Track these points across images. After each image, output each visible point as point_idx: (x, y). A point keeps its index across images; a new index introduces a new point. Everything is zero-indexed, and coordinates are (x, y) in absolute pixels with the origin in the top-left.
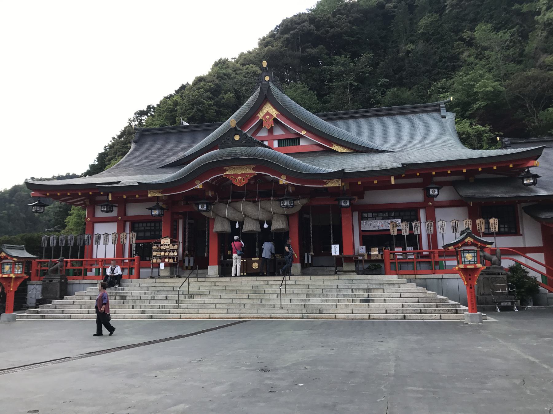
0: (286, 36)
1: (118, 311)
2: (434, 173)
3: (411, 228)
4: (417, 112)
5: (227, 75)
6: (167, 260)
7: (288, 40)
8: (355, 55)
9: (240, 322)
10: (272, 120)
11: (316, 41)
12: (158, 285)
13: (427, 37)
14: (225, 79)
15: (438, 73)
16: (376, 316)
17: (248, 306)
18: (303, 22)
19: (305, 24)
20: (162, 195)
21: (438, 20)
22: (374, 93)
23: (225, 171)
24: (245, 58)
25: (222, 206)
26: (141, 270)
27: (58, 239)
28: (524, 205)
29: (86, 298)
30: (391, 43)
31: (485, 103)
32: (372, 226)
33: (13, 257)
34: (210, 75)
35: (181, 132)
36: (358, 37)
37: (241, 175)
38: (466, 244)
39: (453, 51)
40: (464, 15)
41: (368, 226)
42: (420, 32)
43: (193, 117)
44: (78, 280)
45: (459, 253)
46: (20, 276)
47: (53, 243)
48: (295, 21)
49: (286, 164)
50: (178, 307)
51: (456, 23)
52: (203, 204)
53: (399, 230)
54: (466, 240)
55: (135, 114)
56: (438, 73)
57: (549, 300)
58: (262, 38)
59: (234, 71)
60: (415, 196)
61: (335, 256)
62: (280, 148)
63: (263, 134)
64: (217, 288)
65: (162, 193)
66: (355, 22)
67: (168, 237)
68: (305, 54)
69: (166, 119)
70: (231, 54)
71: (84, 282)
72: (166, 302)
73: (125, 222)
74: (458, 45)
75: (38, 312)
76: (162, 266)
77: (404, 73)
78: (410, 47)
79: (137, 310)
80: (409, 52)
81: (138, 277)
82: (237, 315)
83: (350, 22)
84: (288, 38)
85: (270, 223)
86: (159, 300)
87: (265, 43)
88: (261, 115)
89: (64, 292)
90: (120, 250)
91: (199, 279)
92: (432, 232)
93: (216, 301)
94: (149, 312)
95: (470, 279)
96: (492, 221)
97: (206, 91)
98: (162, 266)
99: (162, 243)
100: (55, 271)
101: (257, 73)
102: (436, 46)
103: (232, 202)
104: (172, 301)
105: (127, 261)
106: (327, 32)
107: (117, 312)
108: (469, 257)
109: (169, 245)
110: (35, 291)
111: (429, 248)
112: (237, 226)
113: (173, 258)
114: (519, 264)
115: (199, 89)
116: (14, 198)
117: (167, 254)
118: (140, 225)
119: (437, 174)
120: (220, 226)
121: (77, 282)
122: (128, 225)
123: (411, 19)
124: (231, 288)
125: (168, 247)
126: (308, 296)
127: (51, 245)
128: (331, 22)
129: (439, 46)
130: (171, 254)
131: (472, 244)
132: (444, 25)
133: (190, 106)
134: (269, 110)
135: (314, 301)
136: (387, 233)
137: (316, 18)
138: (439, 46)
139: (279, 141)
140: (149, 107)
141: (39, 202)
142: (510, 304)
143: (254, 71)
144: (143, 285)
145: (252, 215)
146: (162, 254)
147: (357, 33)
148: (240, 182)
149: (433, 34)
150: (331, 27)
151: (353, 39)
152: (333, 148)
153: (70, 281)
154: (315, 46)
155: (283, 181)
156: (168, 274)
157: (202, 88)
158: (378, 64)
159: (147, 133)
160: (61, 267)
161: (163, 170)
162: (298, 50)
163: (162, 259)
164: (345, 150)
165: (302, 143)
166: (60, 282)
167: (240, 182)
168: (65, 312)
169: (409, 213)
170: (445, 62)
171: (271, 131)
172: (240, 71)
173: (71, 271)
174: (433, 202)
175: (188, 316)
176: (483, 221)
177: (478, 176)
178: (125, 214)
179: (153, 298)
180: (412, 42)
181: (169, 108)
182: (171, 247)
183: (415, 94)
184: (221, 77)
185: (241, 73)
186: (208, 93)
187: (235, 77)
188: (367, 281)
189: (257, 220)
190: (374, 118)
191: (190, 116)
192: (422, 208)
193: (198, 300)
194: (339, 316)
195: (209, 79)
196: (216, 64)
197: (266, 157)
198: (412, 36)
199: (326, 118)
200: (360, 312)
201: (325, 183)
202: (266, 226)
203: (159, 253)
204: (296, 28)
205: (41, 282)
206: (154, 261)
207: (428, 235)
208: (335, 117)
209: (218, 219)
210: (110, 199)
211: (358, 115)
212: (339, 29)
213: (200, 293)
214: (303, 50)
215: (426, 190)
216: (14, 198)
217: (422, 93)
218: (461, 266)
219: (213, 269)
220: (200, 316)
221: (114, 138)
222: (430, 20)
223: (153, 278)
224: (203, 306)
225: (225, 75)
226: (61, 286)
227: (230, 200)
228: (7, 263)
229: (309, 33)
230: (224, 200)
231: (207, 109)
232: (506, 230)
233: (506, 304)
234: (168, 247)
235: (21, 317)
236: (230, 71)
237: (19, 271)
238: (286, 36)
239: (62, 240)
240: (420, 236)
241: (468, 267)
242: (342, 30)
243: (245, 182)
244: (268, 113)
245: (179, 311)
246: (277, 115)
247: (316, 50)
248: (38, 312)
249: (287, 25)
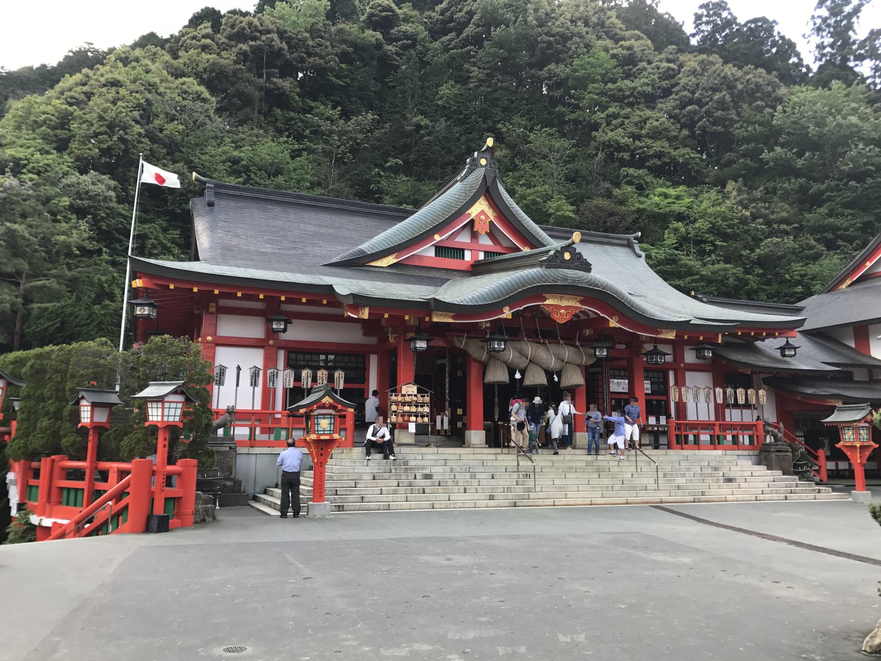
2: (283, 298)
20: (453, 321)
28: (763, 376)
29: (366, 478)
35: (240, 197)
36: (346, 82)
38: (323, 407)
43: (109, 149)
45: (312, 418)
46: (867, 444)
54: (324, 401)
65: (453, 318)
85: (523, 373)
90: (268, 395)
95: (321, 455)
96: (761, 392)
99: (404, 392)
101: (203, 96)
105: (279, 416)
107: (452, 498)
108: (324, 424)
109: (415, 396)
117: (414, 409)
119: (289, 301)
120: (498, 375)
122: (281, 354)
128: (308, 45)
130: (420, 409)
131: (331, 407)
143: (197, 93)
148: (561, 317)
150: (309, 55)
167: (561, 317)
168: (365, 500)
174: (277, 339)
176: (310, 372)
191: (105, 146)
199: (552, 233)
201: (659, 333)
202: (518, 376)
210: (720, 342)
215: (269, 321)
218: (314, 437)
219: (477, 436)
228: (324, 415)
234: (415, 399)
241: (322, 438)
242: (326, 63)
243: (568, 317)
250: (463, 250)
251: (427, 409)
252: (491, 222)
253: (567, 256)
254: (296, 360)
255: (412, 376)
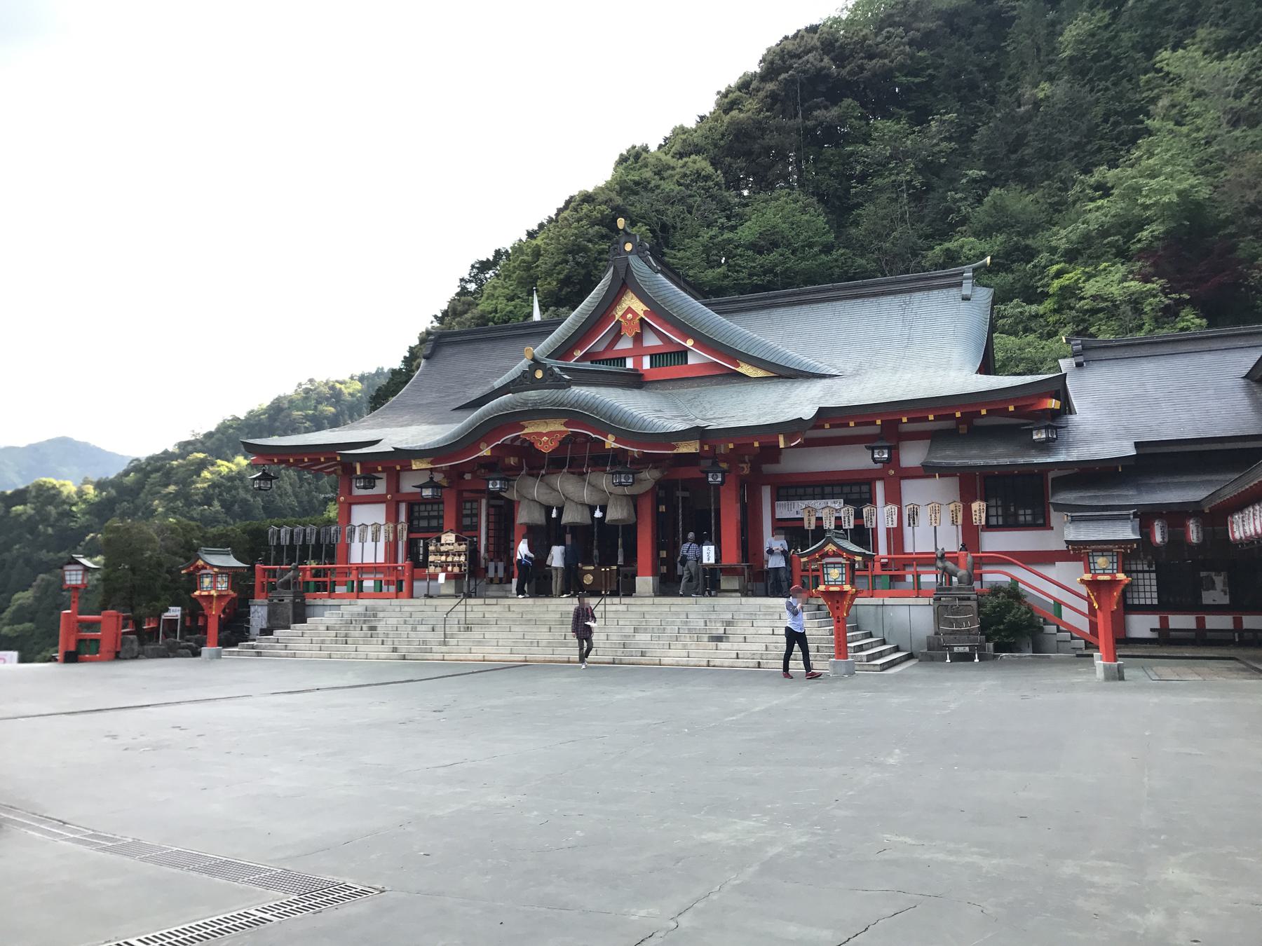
0: (771, 86)
1: (361, 648)
3: (858, 515)
4: (920, 289)
5: (642, 185)
6: (450, 568)
7: (773, 96)
8: (920, 118)
9: (525, 665)
10: (637, 321)
11: (834, 90)
12: (426, 609)
13: (1079, 68)
14: (637, 193)
15: (1100, 150)
16: (717, 662)
17: (543, 643)
18: (810, 51)
19: (810, 57)
21: (1107, 26)
22: (955, 201)
23: (523, 428)
24: (684, 141)
25: (530, 480)
26: (416, 584)
27: (292, 532)
30: (1006, 81)
31: (1162, 229)
32: (794, 510)
33: (213, 566)
34: (608, 187)
37: (547, 434)
39: (1138, 96)
40: (1168, 11)
41: (787, 511)
42: (1065, 54)
44: (321, 600)
47: (285, 540)
48: (789, 52)
49: (610, 418)
50: (445, 643)
51: (1148, 31)
52: (494, 479)
53: (819, 519)
55: (473, 267)
56: (1100, 150)
57: (1061, 644)
58: (723, 91)
59: (658, 173)
60: (856, 460)
61: (707, 565)
62: (655, 370)
63: (625, 344)
64: (510, 615)
66: (926, 40)
67: (452, 531)
68: (810, 123)
69: (519, 283)
70: (652, 136)
71: (330, 602)
72: (431, 635)
73: (398, 503)
74: (1148, 82)
75: (253, 647)
76: (442, 578)
77: (1029, 151)
78: (1044, 90)
79: (388, 646)
80: (1037, 104)
81: (412, 597)
82: (521, 657)
83: (910, 43)
84: (773, 92)
85: (603, 509)
86: (423, 632)
87: (729, 102)
88: (618, 313)
89: (300, 616)
91: (488, 601)
92: (895, 525)
93: (500, 635)
94: (403, 649)
97: (592, 225)
98: (442, 578)
100: (286, 585)
102: (1102, 85)
103: (547, 474)
104: (439, 635)
106: (861, 68)
110: (259, 614)
111: (889, 553)
112: (554, 515)
113: (460, 566)
114: (1015, 581)
115: (579, 220)
116: (278, 424)
117: (450, 559)
118: (423, 508)
121: (319, 602)
123: (1053, 24)
124: (529, 616)
125: (451, 547)
126: (636, 630)
127: (283, 543)
128: (870, 46)
129: (1109, 84)
130: (456, 559)
131: (835, 555)
132: (1123, 35)
133: (562, 256)
134: (632, 304)
135: (642, 638)
136: (797, 524)
137: (837, 41)
138: (1109, 84)
139: (654, 358)
140: (498, 253)
141: (264, 473)
142: (967, 649)
144: (406, 609)
145: (578, 497)
146: (443, 558)
147: (928, 67)
148: (546, 446)
149: (1096, 59)
150: (871, 57)
151: (917, 80)
152: (739, 370)
153: (309, 601)
154: (834, 100)
155: (610, 442)
156: (452, 591)
157: (587, 216)
158: (973, 130)
159: (448, 339)
160: (295, 578)
161: (459, 413)
162: (796, 115)
163: (443, 566)
164: (761, 373)
165: (692, 360)
166: (293, 602)
167: (546, 446)
169: (857, 490)
170: (1116, 124)
171: (638, 338)
172: (670, 172)
173: (312, 586)
175: (454, 656)
177: (978, 422)
178: (398, 490)
179: (414, 629)
180: (1051, 78)
181: (524, 261)
182: (456, 547)
183: (1041, 201)
184: (628, 188)
185: (672, 176)
186: (597, 227)
187: (657, 187)
188: (734, 608)
189: (583, 504)
190: (839, 303)
191: (561, 276)
192: (879, 479)
193: (476, 634)
194: (665, 660)
195: (601, 198)
196: (623, 160)
197: (579, 406)
198: (1051, 62)
199: (720, 307)
200: (701, 653)
201: (674, 447)
202: (598, 514)
203: (438, 557)
204: (791, 67)
205: (266, 602)
206: (432, 569)
207: (888, 530)
208: (768, 302)
209: (524, 504)
211: (811, 297)
212: (886, 61)
213: (483, 623)
214: (807, 115)
216: (278, 424)
217: (1056, 199)
220: (470, 656)
221: (436, 317)
222: (1087, 27)
223: (431, 597)
224: (479, 643)
225: (637, 183)
226: (294, 608)
227: (543, 472)
229: (820, 76)
230: (534, 472)
231: (596, 259)
232: (1029, 518)
233: (961, 649)
234: (451, 547)
235: (231, 653)
236: (647, 174)
237: (223, 585)
238: (771, 86)
239: (298, 534)
240: (875, 530)
242: (892, 61)
243: (554, 445)
244: (630, 310)
245: (444, 649)
246: (645, 312)
247: (835, 111)
248: (253, 647)
249: (772, 63)
250: (625, 358)
251: (463, 558)
252: (642, 320)
253: (539, 374)
254: (860, 493)
255: (453, 526)
